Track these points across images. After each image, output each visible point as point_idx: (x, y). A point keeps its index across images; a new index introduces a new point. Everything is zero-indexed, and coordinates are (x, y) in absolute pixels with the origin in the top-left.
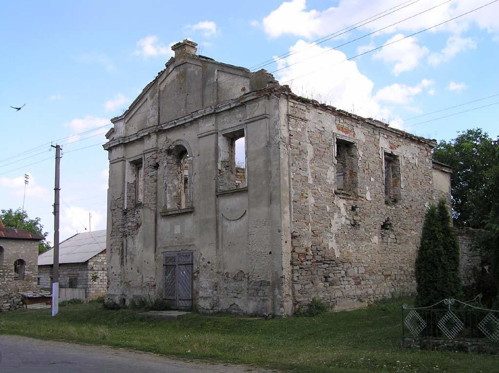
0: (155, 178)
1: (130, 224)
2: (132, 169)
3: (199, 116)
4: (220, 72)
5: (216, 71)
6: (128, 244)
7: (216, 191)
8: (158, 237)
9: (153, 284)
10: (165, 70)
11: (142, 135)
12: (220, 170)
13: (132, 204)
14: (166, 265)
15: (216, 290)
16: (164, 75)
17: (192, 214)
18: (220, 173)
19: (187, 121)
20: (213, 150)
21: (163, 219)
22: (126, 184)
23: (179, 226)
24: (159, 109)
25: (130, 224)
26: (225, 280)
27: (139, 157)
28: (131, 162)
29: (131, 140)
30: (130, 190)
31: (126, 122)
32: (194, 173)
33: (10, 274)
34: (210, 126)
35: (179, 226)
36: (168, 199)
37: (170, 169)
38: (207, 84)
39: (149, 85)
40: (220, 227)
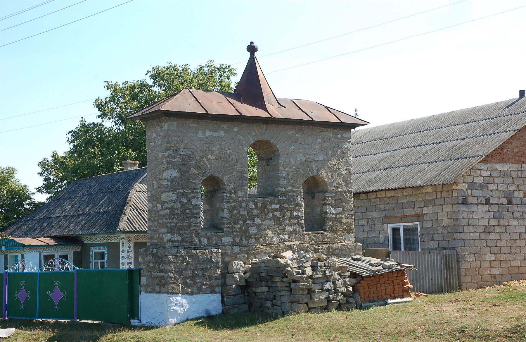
33: (295, 213)
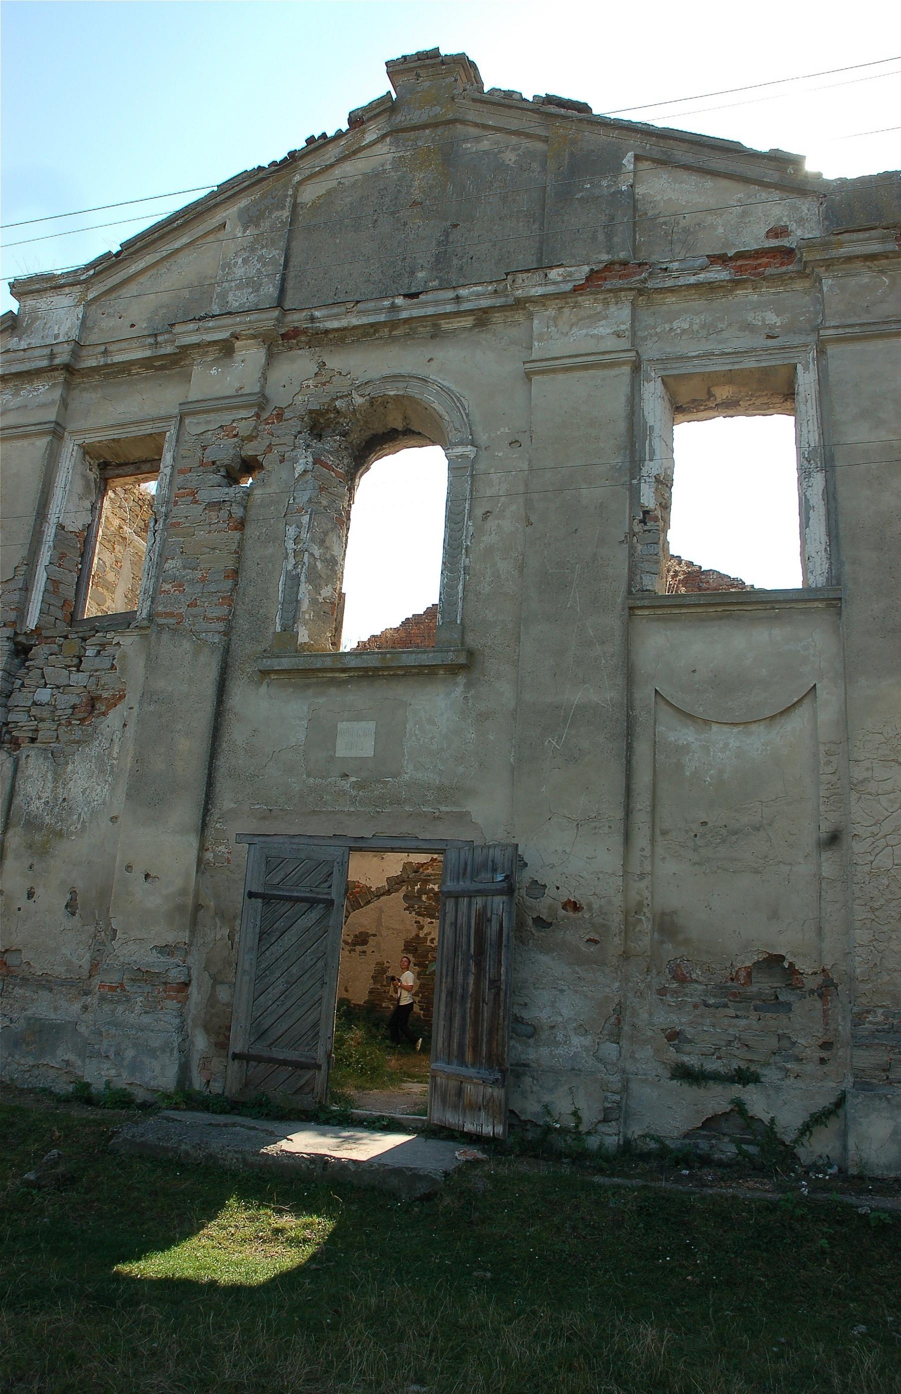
0: (238, 511)
1: (43, 695)
2: (84, 477)
3: (551, 289)
4: (645, 165)
5: (630, 154)
6: (20, 782)
7: (630, 592)
8: (223, 763)
9: (176, 975)
10: (340, 135)
11: (194, 339)
12: (646, 513)
13: (59, 614)
14: (266, 898)
15: (616, 1037)
16: (332, 153)
17: (461, 679)
18: (643, 521)
19: (465, 306)
20: (622, 426)
21: (263, 689)
22: (50, 532)
23: (372, 725)
24: (286, 265)
25: (43, 695)
26: (662, 992)
27: (147, 429)
28: (87, 451)
29: (118, 358)
30: (63, 556)
31: (91, 296)
32: (479, 512)
34: (599, 338)
35: (372, 725)
36: (305, 605)
37: (322, 489)
38: (578, 196)
39: (246, 175)
40: (642, 748)
